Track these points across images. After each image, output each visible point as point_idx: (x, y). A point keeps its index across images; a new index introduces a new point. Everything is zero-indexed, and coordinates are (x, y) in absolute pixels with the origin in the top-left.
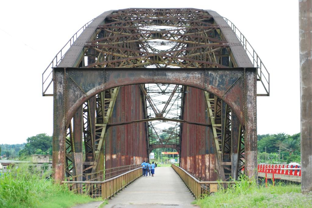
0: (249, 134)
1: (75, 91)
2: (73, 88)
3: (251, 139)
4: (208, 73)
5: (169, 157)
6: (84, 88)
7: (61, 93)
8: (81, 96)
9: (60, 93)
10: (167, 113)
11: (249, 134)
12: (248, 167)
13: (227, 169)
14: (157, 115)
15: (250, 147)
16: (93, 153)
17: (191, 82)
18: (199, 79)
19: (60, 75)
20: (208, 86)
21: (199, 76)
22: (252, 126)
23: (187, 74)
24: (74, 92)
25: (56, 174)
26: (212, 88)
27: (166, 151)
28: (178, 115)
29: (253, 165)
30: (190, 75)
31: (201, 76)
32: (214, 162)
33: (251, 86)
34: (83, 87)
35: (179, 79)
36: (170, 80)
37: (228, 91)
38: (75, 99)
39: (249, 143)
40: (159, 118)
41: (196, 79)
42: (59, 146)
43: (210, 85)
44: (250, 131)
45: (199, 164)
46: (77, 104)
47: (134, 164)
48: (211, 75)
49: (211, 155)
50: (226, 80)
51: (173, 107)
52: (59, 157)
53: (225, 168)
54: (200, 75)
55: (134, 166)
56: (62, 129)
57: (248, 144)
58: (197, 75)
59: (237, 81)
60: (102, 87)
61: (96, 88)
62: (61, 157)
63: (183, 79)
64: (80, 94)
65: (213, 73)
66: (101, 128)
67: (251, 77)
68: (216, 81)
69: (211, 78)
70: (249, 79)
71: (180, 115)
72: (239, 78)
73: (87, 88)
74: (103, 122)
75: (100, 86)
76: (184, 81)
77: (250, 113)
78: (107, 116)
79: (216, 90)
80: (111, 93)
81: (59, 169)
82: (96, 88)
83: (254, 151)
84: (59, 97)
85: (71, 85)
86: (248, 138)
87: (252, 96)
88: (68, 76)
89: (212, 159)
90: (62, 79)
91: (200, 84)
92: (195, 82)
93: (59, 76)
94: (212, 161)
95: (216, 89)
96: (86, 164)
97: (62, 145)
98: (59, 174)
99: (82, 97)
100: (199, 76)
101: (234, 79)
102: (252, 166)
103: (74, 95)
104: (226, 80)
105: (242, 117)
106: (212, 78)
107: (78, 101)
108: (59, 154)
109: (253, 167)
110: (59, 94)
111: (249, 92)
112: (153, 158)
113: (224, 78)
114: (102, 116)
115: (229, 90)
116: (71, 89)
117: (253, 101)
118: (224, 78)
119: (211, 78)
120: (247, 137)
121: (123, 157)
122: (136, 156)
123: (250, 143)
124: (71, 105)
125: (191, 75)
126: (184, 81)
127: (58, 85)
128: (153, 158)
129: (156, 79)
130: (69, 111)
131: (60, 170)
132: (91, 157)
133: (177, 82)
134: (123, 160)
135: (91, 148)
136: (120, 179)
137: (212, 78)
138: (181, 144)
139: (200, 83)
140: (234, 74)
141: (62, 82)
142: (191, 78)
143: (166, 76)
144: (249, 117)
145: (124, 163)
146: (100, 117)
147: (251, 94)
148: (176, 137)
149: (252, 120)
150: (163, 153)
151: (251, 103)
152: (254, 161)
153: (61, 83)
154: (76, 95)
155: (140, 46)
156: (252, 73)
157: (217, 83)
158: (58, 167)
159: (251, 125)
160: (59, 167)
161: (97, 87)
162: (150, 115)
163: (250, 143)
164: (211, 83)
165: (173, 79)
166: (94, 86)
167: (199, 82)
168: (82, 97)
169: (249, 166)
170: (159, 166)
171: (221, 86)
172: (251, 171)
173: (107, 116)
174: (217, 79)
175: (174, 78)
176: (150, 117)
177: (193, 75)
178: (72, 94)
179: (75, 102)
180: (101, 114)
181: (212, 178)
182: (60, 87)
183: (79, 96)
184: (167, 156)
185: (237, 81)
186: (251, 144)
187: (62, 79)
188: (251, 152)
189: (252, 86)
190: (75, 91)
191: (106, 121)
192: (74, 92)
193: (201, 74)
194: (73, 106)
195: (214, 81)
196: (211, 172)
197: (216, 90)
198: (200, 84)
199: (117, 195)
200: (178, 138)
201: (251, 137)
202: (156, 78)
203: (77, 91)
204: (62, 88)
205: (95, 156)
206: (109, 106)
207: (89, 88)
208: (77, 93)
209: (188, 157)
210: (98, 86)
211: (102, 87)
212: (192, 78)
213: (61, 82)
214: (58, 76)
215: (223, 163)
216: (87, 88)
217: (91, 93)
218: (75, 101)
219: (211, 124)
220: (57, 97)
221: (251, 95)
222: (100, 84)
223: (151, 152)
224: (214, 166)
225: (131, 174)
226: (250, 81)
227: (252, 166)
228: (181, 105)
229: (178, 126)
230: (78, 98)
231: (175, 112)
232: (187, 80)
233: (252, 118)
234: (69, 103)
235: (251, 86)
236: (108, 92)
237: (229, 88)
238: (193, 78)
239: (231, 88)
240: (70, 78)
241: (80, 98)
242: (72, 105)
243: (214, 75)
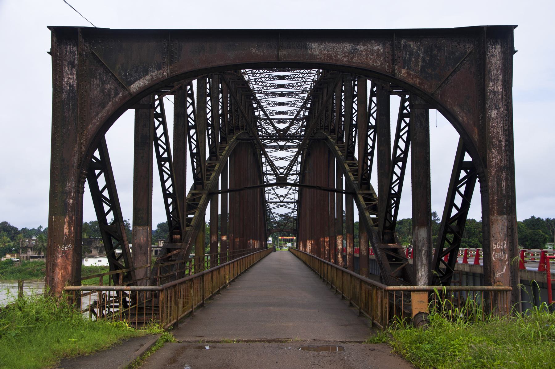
0: (494, 177)
1: (103, 83)
2: (100, 75)
3: (499, 189)
4: (400, 43)
5: (285, 242)
6: (125, 75)
7: (73, 86)
8: (117, 94)
9: (71, 86)
10: (285, 198)
11: (494, 177)
12: (494, 252)
13: (392, 254)
14: (278, 178)
15: (496, 208)
16: (181, 230)
17: (362, 63)
18: (379, 56)
19: (71, 50)
20: (400, 72)
21: (379, 50)
22: (501, 160)
23: (352, 45)
24: (103, 85)
25: (57, 269)
26: (408, 73)
27: (283, 236)
28: (295, 200)
29: (505, 246)
30: (361, 47)
31: (384, 49)
32: (352, 245)
33: (497, 71)
34: (123, 74)
35: (336, 56)
36: (315, 57)
37: (444, 82)
38: (104, 99)
39: (493, 197)
40: (281, 182)
41: (372, 55)
42: (66, 204)
43: (404, 68)
44: (496, 171)
45: (325, 248)
46: (108, 112)
47: (251, 248)
48: (405, 46)
49: (349, 235)
50: (440, 56)
51: (291, 191)
52: (66, 231)
53: (389, 253)
54: (380, 48)
55: (250, 250)
56: (73, 166)
57: (493, 199)
58: (376, 48)
59: (464, 60)
60: (165, 74)
61: (151, 75)
62: (70, 229)
63: (345, 57)
64: (116, 89)
65: (411, 44)
66: (200, 196)
67: (496, 50)
68: (417, 61)
69: (406, 54)
70: (492, 55)
71: (297, 199)
72: (468, 52)
73: (132, 76)
74: (203, 188)
75: (159, 72)
76: (346, 59)
77: (495, 131)
78: (210, 181)
79: (418, 80)
80: (218, 154)
81: (66, 256)
82: (151, 75)
83: (506, 216)
84: (69, 95)
85: (96, 69)
86: (493, 187)
87: (498, 92)
88: (88, 48)
89: (350, 240)
90: (76, 56)
91: (383, 66)
92: (370, 63)
93: (68, 50)
94: (349, 243)
95: (417, 77)
96: (169, 247)
97: (73, 203)
98: (65, 269)
99: (121, 95)
100: (379, 50)
101: (457, 55)
102: (503, 250)
103: (102, 91)
104: (440, 56)
105: (476, 140)
106: (408, 53)
107: (110, 103)
108: (67, 223)
109: (504, 253)
110: (68, 88)
111: (491, 84)
112: (271, 242)
113: (436, 52)
114: (202, 179)
115: (447, 79)
116: (96, 76)
117: (501, 104)
118: (436, 52)
119: (406, 54)
120: (490, 184)
121: (237, 240)
122: (253, 239)
123: (495, 198)
124: (94, 114)
125: (362, 47)
126: (346, 59)
127: (67, 69)
128: (271, 242)
129: (285, 54)
130: (90, 126)
131: (68, 259)
132: (178, 237)
133: (331, 61)
134: (238, 243)
135: (177, 221)
136: (214, 277)
137: (408, 53)
138: (298, 228)
139: (381, 64)
140: (458, 43)
141: (76, 62)
142: (361, 54)
143: (306, 49)
144: (494, 140)
145: (238, 246)
146: (199, 180)
147: (497, 87)
148: (294, 221)
149: (500, 146)
150: (280, 238)
151: (497, 108)
152: (506, 238)
153: (73, 65)
154: (106, 91)
155: (255, 106)
156: (499, 41)
157: (420, 64)
158: (63, 253)
159: (499, 157)
160: (64, 252)
161: (153, 74)
162: (268, 200)
163: (495, 198)
164: (406, 64)
165: (323, 56)
166: (146, 72)
167: (379, 63)
168: (121, 95)
169: (495, 250)
170: (88, 278)
171: (430, 71)
172: (501, 260)
173: (210, 181)
174: (419, 55)
175: (324, 55)
176: (268, 201)
177: (366, 47)
178: (98, 89)
179: (104, 107)
180: (200, 177)
181: (349, 265)
182: (72, 74)
183: (112, 93)
184: (283, 241)
185: (464, 60)
186: (498, 199)
187: (76, 56)
188: (499, 218)
189: (499, 71)
190: (104, 81)
191: (208, 187)
192: (103, 85)
193: (384, 45)
194: (100, 115)
195: (413, 60)
196: (348, 258)
197: (418, 80)
198: (383, 66)
199: (213, 301)
200: (295, 222)
201: (497, 183)
202: (283, 53)
203: (109, 82)
204: (75, 76)
205: (186, 234)
206: (214, 169)
207: (136, 75)
208: (108, 86)
209: (308, 241)
210: (156, 72)
211: (165, 74)
212: (364, 53)
213: (74, 62)
214: (66, 48)
215: (383, 245)
216: (132, 76)
217: (140, 88)
218: (103, 105)
219: (355, 190)
220: (64, 96)
221: (495, 90)
222: (159, 68)
223: (269, 237)
224: (352, 249)
225: (244, 261)
226: (493, 60)
227: (503, 250)
228: (298, 198)
229: (295, 210)
230: (110, 97)
231: (292, 196)
232: (352, 58)
233: (500, 142)
234: (91, 109)
235: (497, 71)
236: (215, 153)
237: (448, 76)
238: (366, 54)
239: (451, 75)
240: (93, 53)
241: (115, 97)
242: (98, 113)
243: (412, 46)
